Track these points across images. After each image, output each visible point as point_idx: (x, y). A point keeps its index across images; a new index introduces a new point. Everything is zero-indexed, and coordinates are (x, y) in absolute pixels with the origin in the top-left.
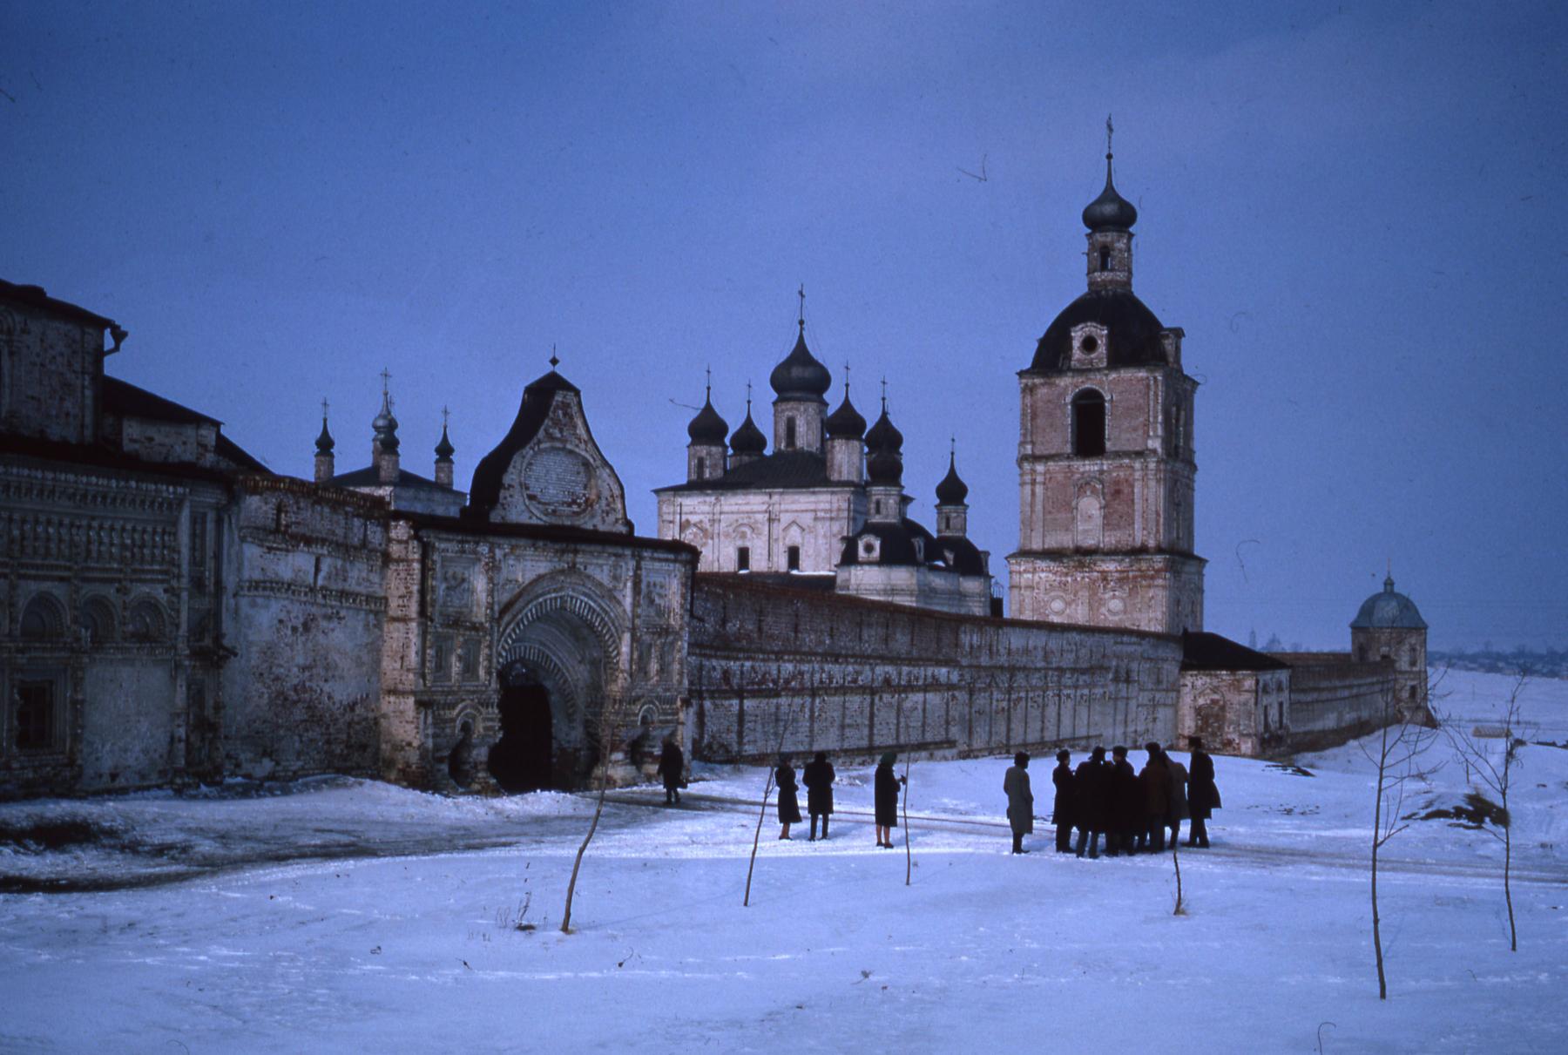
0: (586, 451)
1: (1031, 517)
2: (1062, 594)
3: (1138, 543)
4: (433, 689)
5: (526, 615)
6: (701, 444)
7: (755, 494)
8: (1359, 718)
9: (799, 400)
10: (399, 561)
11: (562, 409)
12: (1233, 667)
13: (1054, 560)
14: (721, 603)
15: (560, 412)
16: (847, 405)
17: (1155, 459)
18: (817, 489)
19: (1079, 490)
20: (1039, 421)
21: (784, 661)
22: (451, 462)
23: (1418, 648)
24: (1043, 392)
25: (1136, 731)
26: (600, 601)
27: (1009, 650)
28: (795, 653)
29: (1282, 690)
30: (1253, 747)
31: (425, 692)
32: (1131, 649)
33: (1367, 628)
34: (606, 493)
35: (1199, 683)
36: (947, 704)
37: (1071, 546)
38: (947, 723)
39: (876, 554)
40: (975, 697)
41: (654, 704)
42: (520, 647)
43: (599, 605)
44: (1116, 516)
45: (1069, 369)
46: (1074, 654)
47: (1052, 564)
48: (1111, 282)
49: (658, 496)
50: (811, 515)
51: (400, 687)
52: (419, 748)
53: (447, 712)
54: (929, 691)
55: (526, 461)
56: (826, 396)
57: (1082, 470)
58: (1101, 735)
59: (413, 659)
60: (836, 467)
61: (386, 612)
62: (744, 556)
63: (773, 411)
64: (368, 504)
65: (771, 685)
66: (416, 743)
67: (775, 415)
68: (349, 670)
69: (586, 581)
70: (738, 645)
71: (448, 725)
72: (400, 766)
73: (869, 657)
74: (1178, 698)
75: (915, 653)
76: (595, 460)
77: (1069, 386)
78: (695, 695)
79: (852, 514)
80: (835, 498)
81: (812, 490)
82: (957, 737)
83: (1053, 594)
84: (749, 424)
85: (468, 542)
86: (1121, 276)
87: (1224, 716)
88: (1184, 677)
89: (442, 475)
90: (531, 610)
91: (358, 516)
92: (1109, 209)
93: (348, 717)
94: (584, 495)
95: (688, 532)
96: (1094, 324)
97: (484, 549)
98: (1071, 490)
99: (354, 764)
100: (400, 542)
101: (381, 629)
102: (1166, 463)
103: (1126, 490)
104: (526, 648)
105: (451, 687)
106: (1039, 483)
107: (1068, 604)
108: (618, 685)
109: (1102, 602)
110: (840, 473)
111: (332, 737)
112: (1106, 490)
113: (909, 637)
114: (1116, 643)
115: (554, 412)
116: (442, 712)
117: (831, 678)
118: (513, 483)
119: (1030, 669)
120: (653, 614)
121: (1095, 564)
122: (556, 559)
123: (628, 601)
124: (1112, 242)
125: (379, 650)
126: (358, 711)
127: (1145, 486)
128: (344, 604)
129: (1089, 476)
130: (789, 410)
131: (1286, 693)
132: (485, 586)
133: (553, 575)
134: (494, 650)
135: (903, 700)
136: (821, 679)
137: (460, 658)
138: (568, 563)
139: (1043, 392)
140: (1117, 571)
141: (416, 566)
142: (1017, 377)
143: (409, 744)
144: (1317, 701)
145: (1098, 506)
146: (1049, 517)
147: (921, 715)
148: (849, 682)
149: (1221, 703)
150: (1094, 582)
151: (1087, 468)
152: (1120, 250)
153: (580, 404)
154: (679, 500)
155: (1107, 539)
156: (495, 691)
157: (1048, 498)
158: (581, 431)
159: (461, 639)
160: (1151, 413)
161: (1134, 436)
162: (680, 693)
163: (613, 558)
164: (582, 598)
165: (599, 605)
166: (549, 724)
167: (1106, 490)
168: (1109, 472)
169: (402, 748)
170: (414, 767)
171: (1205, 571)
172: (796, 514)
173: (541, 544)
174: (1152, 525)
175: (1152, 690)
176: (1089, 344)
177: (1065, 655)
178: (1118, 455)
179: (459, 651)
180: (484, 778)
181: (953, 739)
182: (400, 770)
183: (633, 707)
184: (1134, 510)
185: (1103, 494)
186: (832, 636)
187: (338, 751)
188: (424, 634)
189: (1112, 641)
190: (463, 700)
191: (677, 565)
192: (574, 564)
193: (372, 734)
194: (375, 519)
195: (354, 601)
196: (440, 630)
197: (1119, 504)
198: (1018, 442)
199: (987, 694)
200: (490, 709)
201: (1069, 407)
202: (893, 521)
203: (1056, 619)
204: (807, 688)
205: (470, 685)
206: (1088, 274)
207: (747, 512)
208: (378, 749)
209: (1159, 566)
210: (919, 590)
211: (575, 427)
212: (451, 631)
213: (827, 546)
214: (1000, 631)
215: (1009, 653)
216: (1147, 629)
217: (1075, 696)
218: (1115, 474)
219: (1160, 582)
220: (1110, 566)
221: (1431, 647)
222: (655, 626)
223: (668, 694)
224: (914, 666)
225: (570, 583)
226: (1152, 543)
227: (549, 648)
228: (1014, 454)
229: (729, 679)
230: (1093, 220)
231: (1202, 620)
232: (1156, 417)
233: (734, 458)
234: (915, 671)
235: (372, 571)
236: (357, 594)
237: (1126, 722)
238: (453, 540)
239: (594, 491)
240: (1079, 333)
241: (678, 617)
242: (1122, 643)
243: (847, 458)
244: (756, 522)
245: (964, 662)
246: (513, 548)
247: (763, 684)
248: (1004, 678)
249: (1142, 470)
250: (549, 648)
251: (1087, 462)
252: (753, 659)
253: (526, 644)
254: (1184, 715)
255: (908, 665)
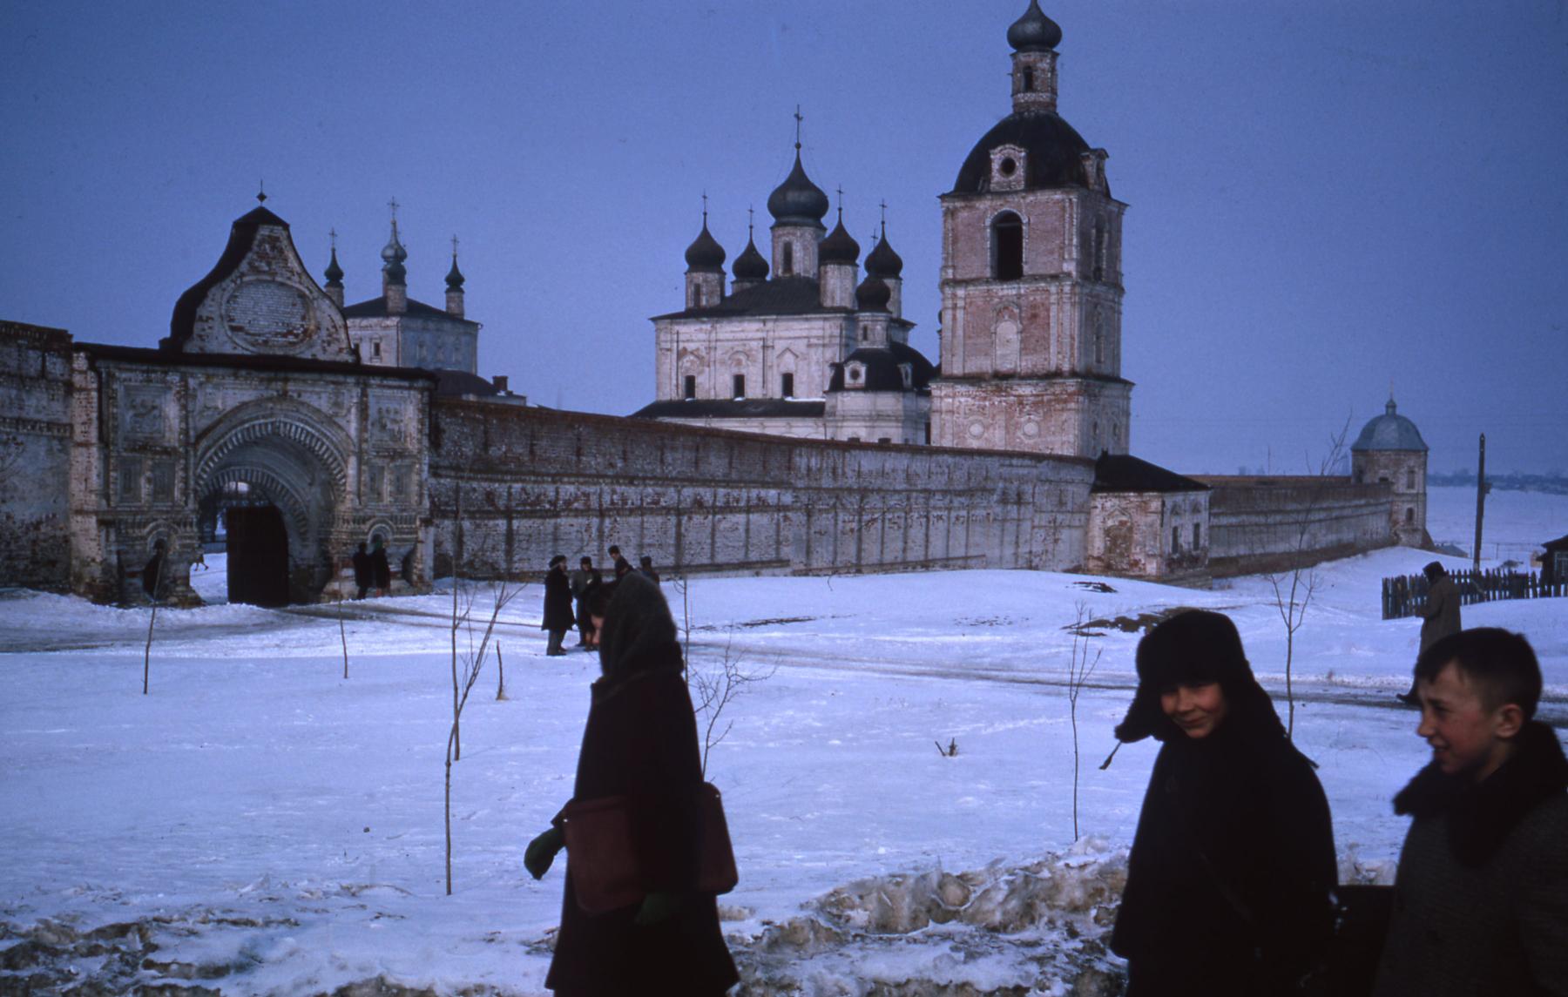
0: (300, 283)
1: (952, 341)
2: (981, 418)
3: (1053, 368)
4: (119, 509)
5: (231, 439)
6: (697, 271)
7: (749, 321)
8: (1339, 540)
9: (795, 225)
10: (81, 390)
11: (269, 243)
12: (1140, 488)
13: (972, 385)
14: (482, 428)
15: (267, 246)
16: (840, 229)
17: (1069, 283)
18: (809, 316)
19: (998, 314)
20: (959, 245)
21: (562, 483)
22: (462, 291)
23: (1416, 469)
24: (964, 215)
25: (1031, 552)
26: (319, 426)
27: (859, 472)
28: (578, 475)
29: (1199, 511)
30: (1159, 568)
31: (108, 511)
32: (1022, 471)
33: (1367, 451)
34: (326, 323)
35: (1108, 504)
36: (778, 525)
37: (990, 371)
38: (778, 543)
39: (862, 380)
40: (814, 518)
41: (388, 524)
42: (240, 471)
43: (318, 430)
44: (1033, 340)
45: (989, 192)
46: (946, 477)
47: (971, 389)
48: (1034, 103)
49: (656, 324)
50: (805, 341)
51: (86, 507)
52: (101, 563)
53: (137, 531)
54: (753, 512)
55: (227, 295)
56: (824, 220)
57: (1000, 294)
58: (984, 556)
59: (95, 482)
60: (829, 294)
61: (71, 437)
62: (739, 382)
63: (770, 237)
64: (45, 337)
65: (547, 506)
66: (98, 559)
67: (773, 241)
68: (31, 491)
69: (301, 408)
70: (504, 468)
71: (137, 542)
72: (87, 580)
73: (673, 479)
74: (1088, 520)
75: (734, 476)
76: (311, 292)
77: (987, 209)
78: (438, 511)
79: (844, 340)
80: (827, 324)
81: (804, 316)
82: (791, 557)
83: (971, 418)
84: (751, 248)
85: (155, 372)
86: (1044, 97)
87: (1131, 537)
88: (1094, 499)
89: (453, 305)
90: (236, 435)
91: (34, 348)
92: (1032, 28)
93: (32, 535)
94: (302, 326)
95: (685, 360)
96: (1012, 146)
97: (174, 378)
98: (992, 314)
99: (41, 579)
100: (81, 372)
101: (67, 454)
102: (1082, 286)
103: (1043, 314)
104: (247, 471)
105: (139, 507)
106: (960, 308)
107: (986, 428)
108: (347, 505)
109: (1017, 426)
110: (833, 298)
111: (14, 554)
112: (1023, 315)
113: (727, 460)
114: (1002, 465)
115: (259, 246)
116: (130, 531)
117: (625, 501)
118: (213, 316)
119: (888, 491)
120: (386, 438)
121: (1011, 388)
122: (263, 387)
123: (353, 428)
124: (1035, 62)
125: (66, 474)
126: (43, 529)
127: (1061, 310)
128: (21, 431)
129: (1007, 300)
130: (787, 235)
131: (1204, 515)
132: (177, 413)
133: (258, 403)
134: (191, 473)
135: (720, 521)
136: (612, 500)
137: (149, 481)
138: (277, 391)
139: (964, 215)
140: (1032, 395)
141: (94, 394)
142: (939, 200)
143: (93, 560)
144: (1281, 524)
145: (1015, 330)
146: (969, 342)
147: (743, 535)
148: (648, 503)
149: (1129, 524)
150: (1011, 406)
151: (1005, 292)
152: (1043, 70)
153: (289, 237)
154: (676, 328)
155: (1024, 364)
156: (193, 511)
157: (968, 322)
158: (293, 263)
159: (150, 463)
160: (1066, 236)
161: (1051, 259)
162: (420, 513)
163: (332, 386)
164: (298, 424)
165: (318, 430)
166: (285, 544)
167: (1023, 315)
168: (1026, 295)
169: (88, 565)
170: (98, 581)
171: (1132, 394)
172: (790, 341)
173: (243, 373)
174: (1067, 349)
175: (1052, 511)
176: (1008, 167)
177: (934, 477)
178: (1036, 278)
179: (148, 474)
180: (182, 592)
181: (786, 558)
182: (87, 584)
183: (363, 526)
184: (1049, 335)
185: (1021, 318)
186: (625, 459)
187: (22, 567)
188: (106, 459)
189: (997, 465)
190: (155, 520)
191: (412, 392)
192: (285, 393)
193: (61, 551)
194: (54, 351)
195: (33, 428)
196: (124, 454)
197: (1035, 329)
198: (940, 266)
199: (830, 516)
200: (188, 528)
201: (988, 230)
202: (881, 347)
203: (975, 444)
204: (595, 510)
205: (162, 506)
206: (1012, 95)
207: (742, 340)
208: (69, 564)
209: (1071, 389)
210: (905, 416)
211: (286, 260)
212: (137, 455)
213: (820, 373)
214: (847, 454)
215: (859, 474)
216: (1060, 453)
217: (949, 518)
218: (1031, 298)
219: (1073, 405)
220: (1026, 390)
221: (1431, 471)
222: (387, 450)
223: (405, 514)
224: (732, 488)
225: (281, 410)
226: (1066, 367)
227: (274, 471)
228: (937, 281)
229: (493, 501)
230: (1019, 41)
231: (1127, 443)
232: (1071, 240)
233: (735, 285)
234: (735, 493)
235: (53, 399)
236: (36, 422)
237: (1017, 543)
238: (136, 370)
239: (313, 322)
240: (998, 156)
241: (414, 441)
242: (1011, 465)
243: (840, 284)
244: (751, 350)
245: (800, 484)
246: (208, 377)
247: (536, 505)
248: (854, 500)
249: (1058, 293)
250: (274, 471)
251: (1005, 286)
252: (523, 481)
253: (247, 467)
254: (1093, 537)
255: (724, 487)
